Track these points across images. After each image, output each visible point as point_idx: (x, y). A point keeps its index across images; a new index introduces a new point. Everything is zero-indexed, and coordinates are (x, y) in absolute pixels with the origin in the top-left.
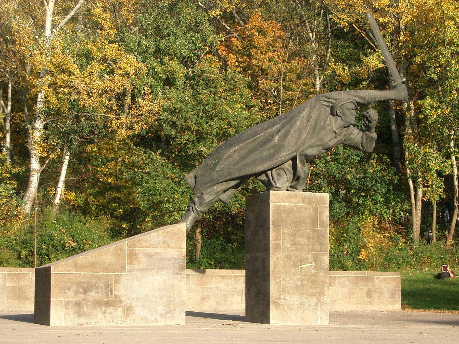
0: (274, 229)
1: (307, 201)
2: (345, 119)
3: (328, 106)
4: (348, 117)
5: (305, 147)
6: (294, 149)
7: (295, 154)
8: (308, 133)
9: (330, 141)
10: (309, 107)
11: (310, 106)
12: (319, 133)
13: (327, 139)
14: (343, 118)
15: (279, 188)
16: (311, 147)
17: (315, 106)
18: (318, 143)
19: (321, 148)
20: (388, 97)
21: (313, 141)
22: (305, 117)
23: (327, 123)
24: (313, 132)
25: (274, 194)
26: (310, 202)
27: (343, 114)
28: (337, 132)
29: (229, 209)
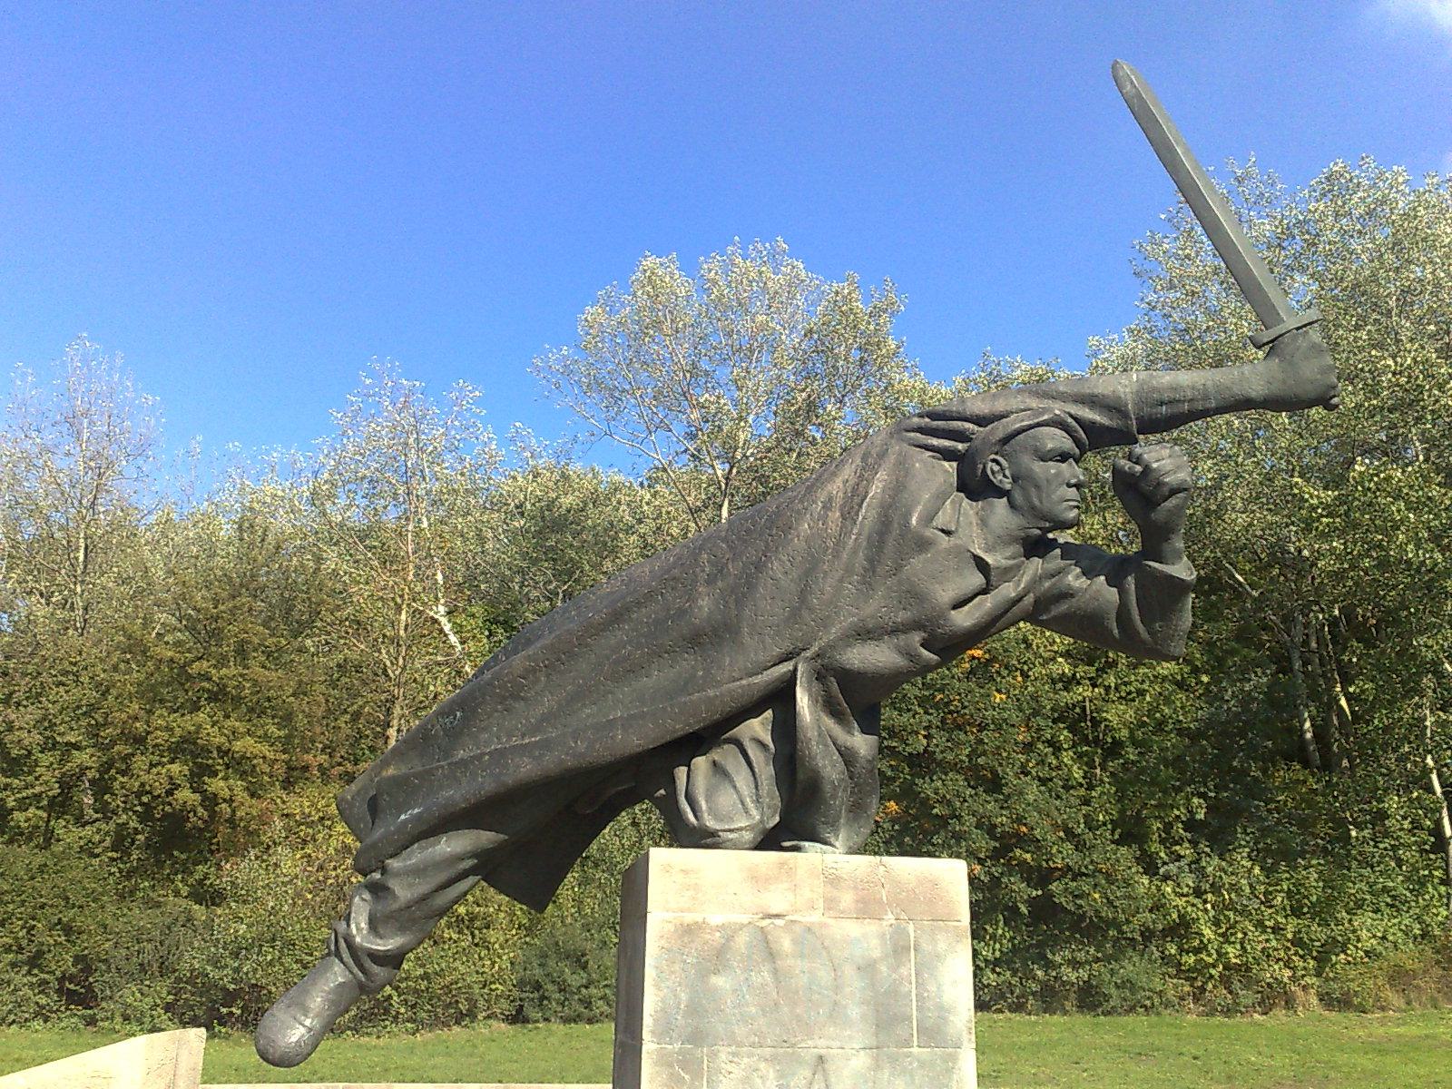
0: (663, 1060)
1: (847, 899)
2: (1027, 498)
3: (947, 455)
4: (1037, 487)
5: (834, 632)
6: (787, 646)
7: (786, 667)
8: (849, 570)
9: (958, 605)
10: (858, 461)
11: (864, 459)
12: (898, 569)
13: (945, 593)
14: (1018, 497)
15: (714, 834)
16: (865, 634)
17: (882, 455)
18: (902, 616)
19: (917, 637)
20: (1236, 390)
21: (876, 607)
22: (839, 501)
23: (941, 519)
24: (872, 564)
25: (667, 869)
26: (867, 909)
27: (1015, 479)
28: (989, 559)
29: (1288, 651)
